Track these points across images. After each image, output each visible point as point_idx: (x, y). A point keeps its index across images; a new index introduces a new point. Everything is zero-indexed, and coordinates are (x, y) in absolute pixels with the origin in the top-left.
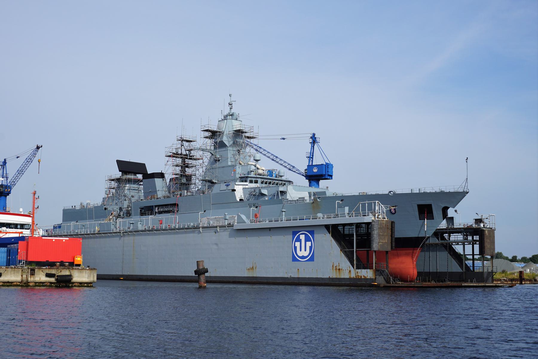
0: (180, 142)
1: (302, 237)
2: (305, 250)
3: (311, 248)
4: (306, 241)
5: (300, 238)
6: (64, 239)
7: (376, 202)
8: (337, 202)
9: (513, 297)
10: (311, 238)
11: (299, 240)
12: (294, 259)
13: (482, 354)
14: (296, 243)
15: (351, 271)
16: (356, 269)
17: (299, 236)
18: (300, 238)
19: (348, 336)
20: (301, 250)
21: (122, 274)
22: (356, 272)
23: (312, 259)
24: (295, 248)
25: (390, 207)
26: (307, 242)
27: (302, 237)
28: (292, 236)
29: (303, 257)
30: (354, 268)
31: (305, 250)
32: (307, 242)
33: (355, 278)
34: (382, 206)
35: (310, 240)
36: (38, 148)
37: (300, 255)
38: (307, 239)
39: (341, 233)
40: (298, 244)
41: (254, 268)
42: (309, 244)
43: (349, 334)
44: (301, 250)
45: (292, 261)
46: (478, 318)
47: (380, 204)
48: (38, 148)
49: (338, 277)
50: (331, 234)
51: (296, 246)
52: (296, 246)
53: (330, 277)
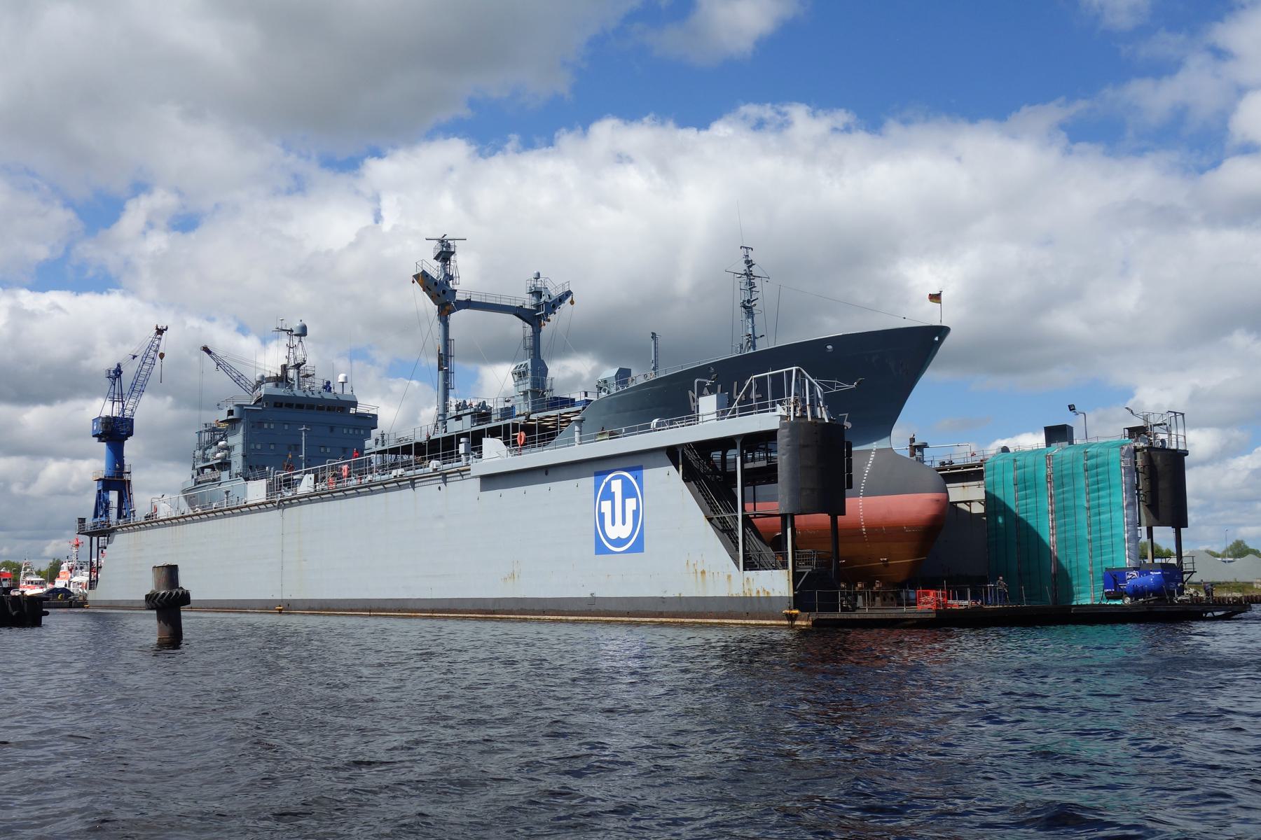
0: (1118, 449)
1: (617, 486)
2: (624, 523)
3: (636, 514)
7: (792, 371)
8: (696, 381)
9: (628, 791)
10: (632, 483)
11: (608, 495)
12: (600, 549)
14: (602, 502)
15: (732, 578)
16: (745, 570)
17: (608, 485)
20: (613, 523)
21: (281, 598)
22: (745, 579)
23: (638, 547)
24: (602, 516)
25: (838, 384)
26: (627, 500)
27: (617, 486)
29: (619, 542)
30: (739, 569)
31: (624, 523)
32: (627, 500)
33: (742, 595)
34: (813, 381)
35: (634, 495)
36: (160, 332)
38: (628, 492)
39: (718, 469)
40: (606, 506)
41: (516, 576)
42: (631, 504)
44: (613, 523)
47: (807, 375)
48: (160, 332)
50: (681, 471)
53: (43, 618)
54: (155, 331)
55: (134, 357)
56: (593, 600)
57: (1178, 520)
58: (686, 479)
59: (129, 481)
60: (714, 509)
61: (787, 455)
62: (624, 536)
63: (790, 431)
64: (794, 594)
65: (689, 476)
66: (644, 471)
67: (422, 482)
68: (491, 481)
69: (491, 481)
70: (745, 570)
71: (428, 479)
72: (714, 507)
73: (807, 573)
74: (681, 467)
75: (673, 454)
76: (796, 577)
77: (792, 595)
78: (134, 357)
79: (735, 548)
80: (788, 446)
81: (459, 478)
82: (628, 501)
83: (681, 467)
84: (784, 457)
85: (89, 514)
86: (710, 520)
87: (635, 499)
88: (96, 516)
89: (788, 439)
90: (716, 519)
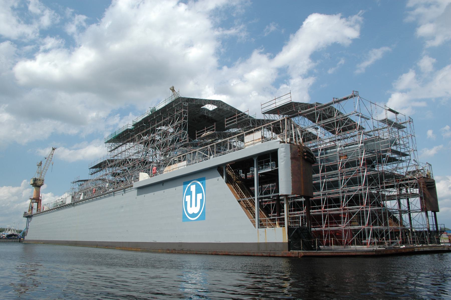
2: (196, 206)
3: (202, 201)
4: (197, 193)
5: (191, 190)
6: (273, 299)
10: (202, 189)
11: (189, 193)
13: (267, 256)
16: (258, 228)
17: (189, 188)
18: (191, 190)
19: (15, 273)
20: (191, 207)
24: (186, 203)
27: (193, 188)
28: (221, 177)
29: (193, 215)
31: (196, 206)
37: (190, 212)
38: (198, 190)
40: (188, 198)
42: (200, 196)
43: (233, 267)
44: (191, 207)
45: (205, 219)
46: (138, 248)
49: (439, 202)
51: (186, 201)
52: (186, 201)
54: (52, 149)
55: (46, 158)
56: (180, 244)
57: (435, 209)
58: (227, 182)
59: (41, 200)
60: (242, 197)
61: (284, 162)
62: (196, 212)
63: (285, 149)
64: (288, 241)
65: (229, 181)
66: (206, 181)
67: (120, 192)
68: (143, 189)
69: (143, 189)
70: (258, 228)
71: (119, 191)
72: (242, 196)
73: (296, 229)
74: (224, 176)
75: (220, 169)
76: (290, 230)
77: (287, 241)
78: (46, 158)
79: (253, 217)
80: (284, 157)
81: (130, 190)
82: (198, 195)
83: (224, 176)
84: (283, 163)
85: (27, 210)
86: (239, 202)
87: (201, 194)
88: (29, 211)
89: (284, 153)
90: (242, 202)
